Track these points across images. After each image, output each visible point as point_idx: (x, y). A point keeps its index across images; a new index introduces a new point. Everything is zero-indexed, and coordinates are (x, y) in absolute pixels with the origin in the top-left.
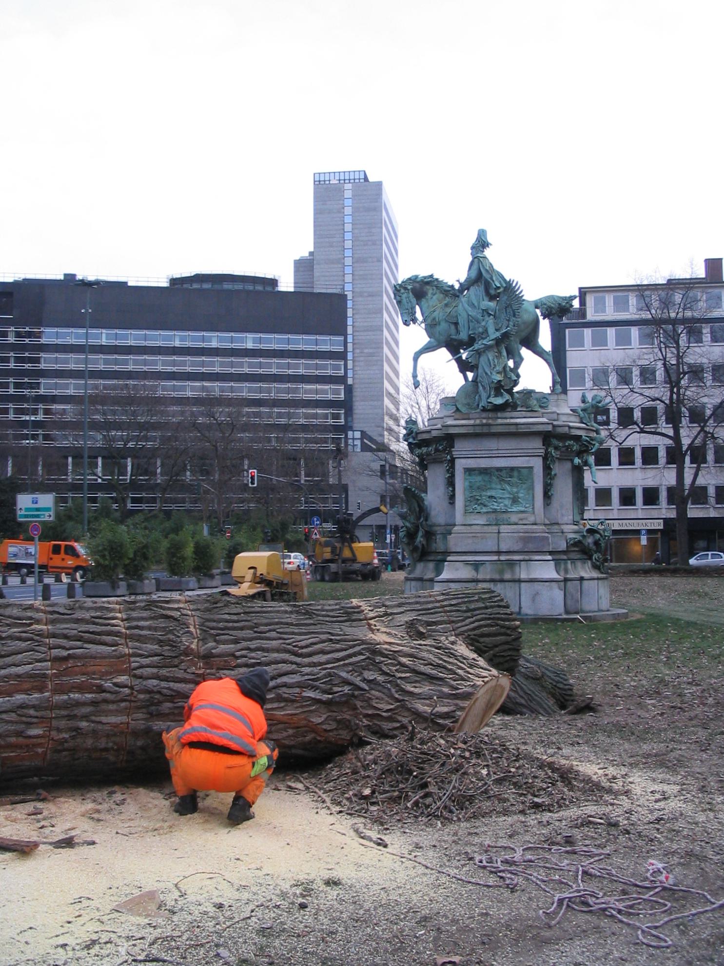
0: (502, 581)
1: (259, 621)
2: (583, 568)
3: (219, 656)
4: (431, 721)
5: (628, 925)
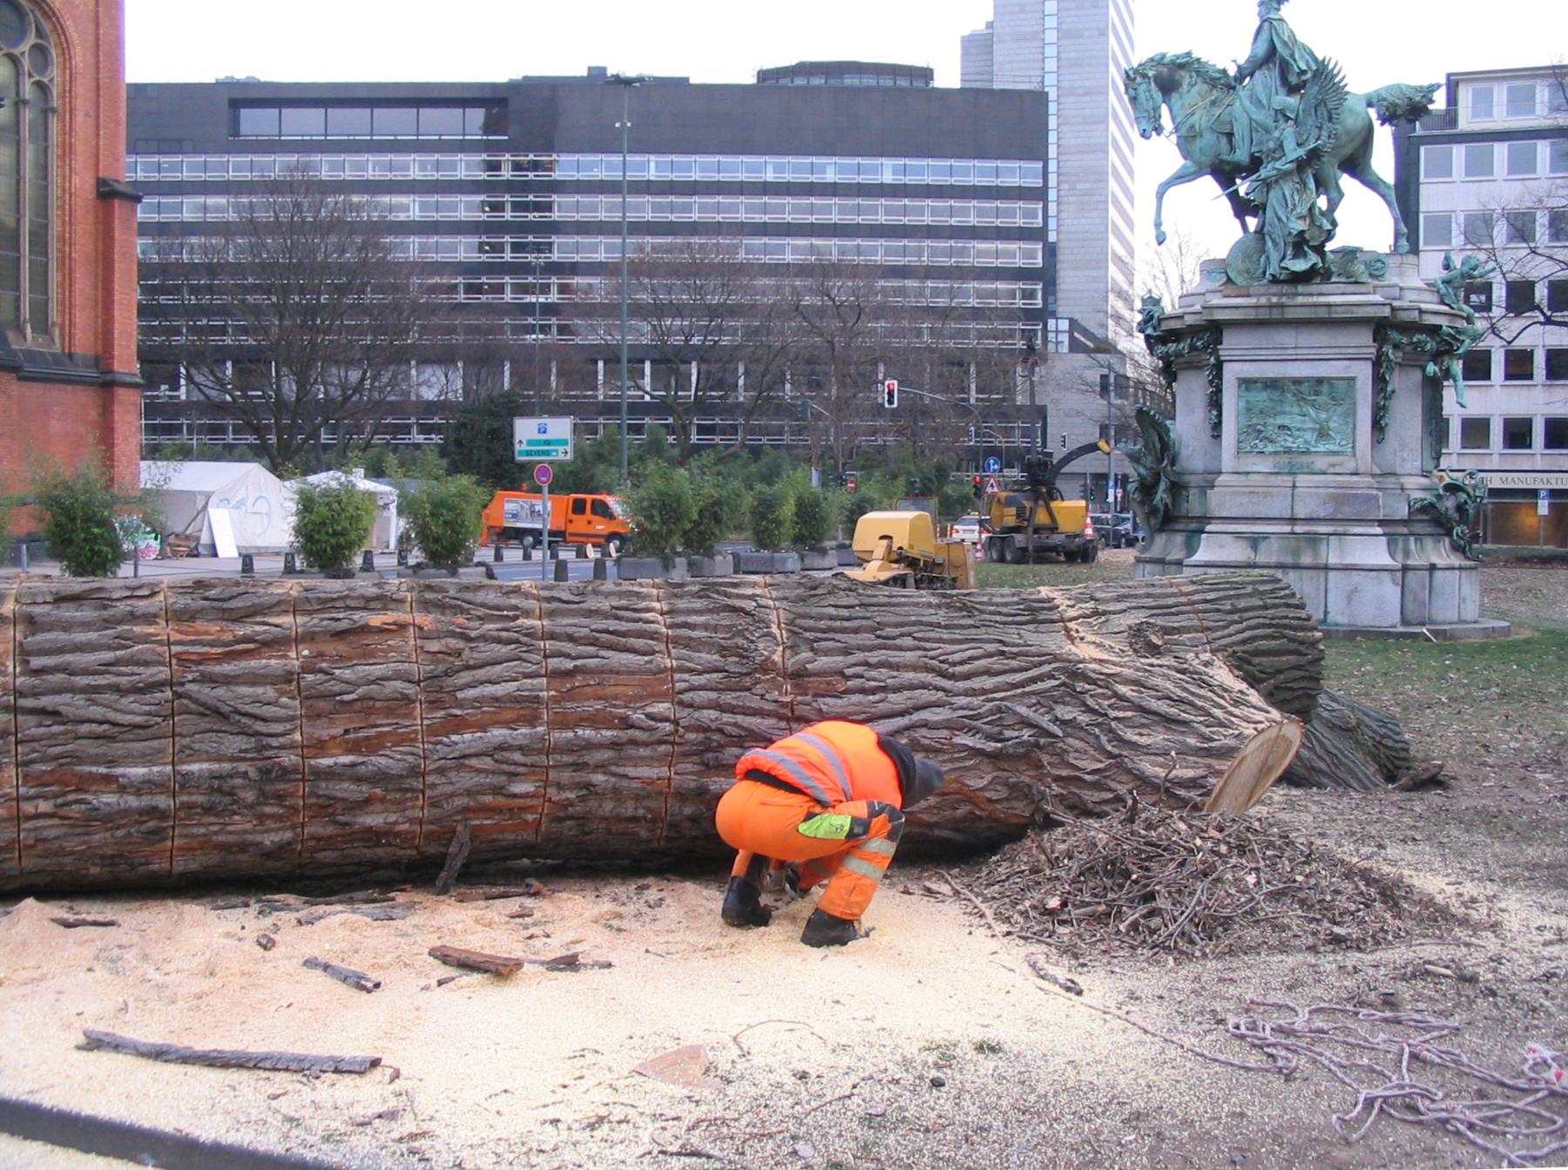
0: (1296, 567)
1: (885, 619)
2: (1436, 549)
3: (818, 674)
4: (1167, 792)
5: (1486, 1150)
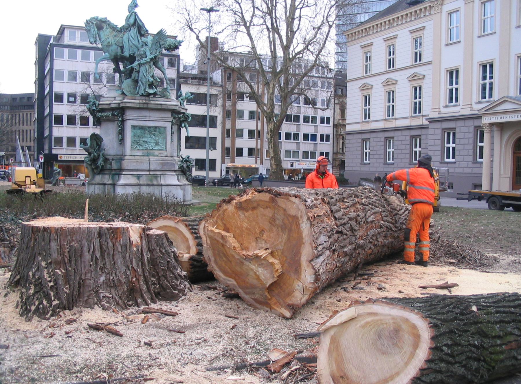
0: (153, 185)
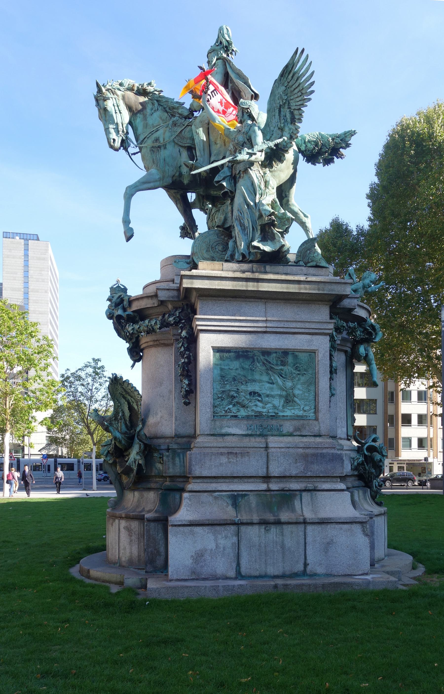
0: (278, 523)
